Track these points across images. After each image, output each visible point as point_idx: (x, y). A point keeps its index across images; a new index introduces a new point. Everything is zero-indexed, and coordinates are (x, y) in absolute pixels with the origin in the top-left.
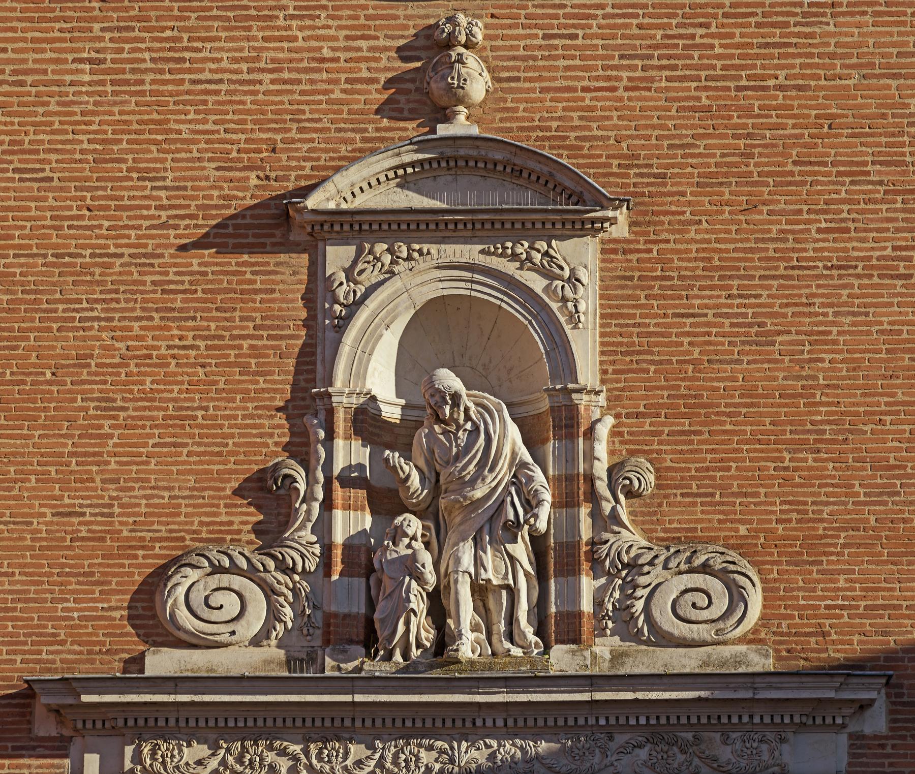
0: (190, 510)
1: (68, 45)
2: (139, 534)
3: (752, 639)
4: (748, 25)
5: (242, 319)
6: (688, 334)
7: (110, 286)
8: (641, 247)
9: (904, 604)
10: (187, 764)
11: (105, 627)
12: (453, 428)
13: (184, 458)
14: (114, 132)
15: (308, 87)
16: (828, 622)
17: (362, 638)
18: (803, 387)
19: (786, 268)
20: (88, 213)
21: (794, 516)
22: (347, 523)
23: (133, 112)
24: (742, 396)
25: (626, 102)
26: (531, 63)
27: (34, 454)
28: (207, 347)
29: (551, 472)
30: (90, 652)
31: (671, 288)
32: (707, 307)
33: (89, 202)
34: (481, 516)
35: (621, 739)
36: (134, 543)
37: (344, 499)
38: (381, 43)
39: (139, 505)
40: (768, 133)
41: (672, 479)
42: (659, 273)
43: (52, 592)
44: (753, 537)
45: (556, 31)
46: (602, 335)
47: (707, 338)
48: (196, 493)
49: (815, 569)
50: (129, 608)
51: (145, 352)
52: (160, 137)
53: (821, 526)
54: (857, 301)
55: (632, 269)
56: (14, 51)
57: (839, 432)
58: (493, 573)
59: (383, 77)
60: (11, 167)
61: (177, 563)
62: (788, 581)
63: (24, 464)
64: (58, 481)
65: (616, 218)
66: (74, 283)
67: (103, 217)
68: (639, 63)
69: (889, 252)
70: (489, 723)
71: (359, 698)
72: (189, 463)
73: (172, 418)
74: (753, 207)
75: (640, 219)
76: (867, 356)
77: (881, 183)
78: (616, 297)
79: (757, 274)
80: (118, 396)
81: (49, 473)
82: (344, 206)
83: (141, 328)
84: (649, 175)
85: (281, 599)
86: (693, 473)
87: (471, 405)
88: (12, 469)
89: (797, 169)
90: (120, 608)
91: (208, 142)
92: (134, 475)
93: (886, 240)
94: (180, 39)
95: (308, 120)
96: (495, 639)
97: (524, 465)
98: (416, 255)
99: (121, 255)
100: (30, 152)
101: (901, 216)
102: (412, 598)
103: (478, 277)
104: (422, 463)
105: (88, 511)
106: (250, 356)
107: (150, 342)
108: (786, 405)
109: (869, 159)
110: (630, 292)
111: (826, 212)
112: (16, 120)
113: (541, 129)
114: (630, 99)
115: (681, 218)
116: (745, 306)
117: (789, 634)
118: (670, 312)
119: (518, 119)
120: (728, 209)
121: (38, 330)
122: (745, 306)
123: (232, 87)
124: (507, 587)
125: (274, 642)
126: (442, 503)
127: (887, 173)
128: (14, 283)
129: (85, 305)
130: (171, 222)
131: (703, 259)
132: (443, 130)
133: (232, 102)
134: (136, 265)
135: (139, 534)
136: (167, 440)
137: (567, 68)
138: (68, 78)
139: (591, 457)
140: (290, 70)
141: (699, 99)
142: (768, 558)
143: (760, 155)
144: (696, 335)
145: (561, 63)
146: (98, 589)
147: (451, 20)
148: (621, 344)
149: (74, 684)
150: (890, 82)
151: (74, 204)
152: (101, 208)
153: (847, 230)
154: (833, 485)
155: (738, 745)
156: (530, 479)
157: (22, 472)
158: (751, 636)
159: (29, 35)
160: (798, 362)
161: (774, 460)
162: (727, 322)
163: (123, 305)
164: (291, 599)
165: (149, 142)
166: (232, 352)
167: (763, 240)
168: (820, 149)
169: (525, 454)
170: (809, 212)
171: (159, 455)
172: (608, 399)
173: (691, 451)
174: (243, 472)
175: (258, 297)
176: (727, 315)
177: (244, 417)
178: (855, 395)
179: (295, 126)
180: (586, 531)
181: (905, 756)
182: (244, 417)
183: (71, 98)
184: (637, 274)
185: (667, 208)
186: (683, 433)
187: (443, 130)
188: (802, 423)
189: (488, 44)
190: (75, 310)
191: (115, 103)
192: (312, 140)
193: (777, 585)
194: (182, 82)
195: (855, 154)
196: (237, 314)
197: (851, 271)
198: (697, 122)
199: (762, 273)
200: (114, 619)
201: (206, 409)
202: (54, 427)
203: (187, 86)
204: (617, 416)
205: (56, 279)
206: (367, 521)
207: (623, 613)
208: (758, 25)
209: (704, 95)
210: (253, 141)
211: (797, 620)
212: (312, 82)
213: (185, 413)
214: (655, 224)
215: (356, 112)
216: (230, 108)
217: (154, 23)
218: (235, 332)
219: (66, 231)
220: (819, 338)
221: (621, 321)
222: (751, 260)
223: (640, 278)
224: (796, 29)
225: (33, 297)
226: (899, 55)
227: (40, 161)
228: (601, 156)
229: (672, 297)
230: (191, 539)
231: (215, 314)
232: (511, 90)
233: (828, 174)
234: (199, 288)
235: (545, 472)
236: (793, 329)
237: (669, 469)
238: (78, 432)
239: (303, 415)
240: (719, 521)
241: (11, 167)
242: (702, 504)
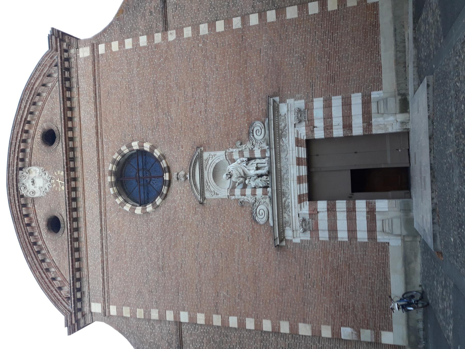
16: (261, 109)
69: (203, 104)
73: (233, 222)
96: (265, 166)
137: (180, 159)
155: (282, 122)
161: (235, 121)
162: (215, 130)
181: (283, 93)
208: (173, 128)
220: (216, 114)
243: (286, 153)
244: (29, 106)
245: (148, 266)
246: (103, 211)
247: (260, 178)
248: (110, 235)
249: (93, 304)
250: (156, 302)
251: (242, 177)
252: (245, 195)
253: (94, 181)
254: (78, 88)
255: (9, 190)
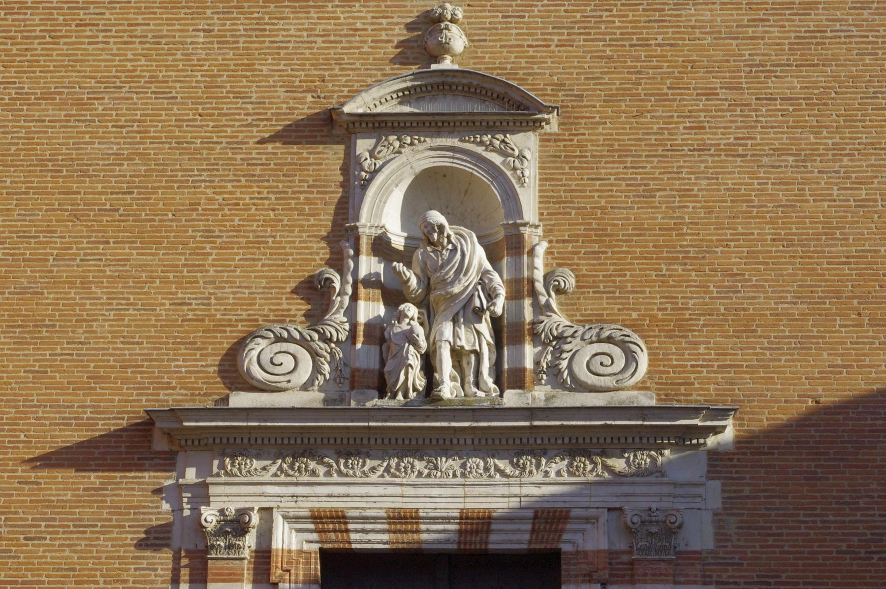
0: (262, 301)
1: (190, 21)
2: (227, 317)
3: (642, 387)
5: (300, 181)
6: (597, 191)
7: (213, 161)
8: (566, 138)
9: (745, 364)
10: (256, 469)
11: (203, 378)
12: (440, 249)
13: (259, 268)
14: (218, 71)
15: (347, 45)
16: (692, 376)
18: (675, 224)
19: (663, 150)
20: (199, 118)
21: (669, 306)
22: (367, 311)
23: (231, 59)
24: (633, 229)
25: (557, 53)
26: (494, 31)
27: (159, 266)
28: (277, 199)
29: (505, 277)
30: (192, 395)
31: (586, 162)
32: (610, 174)
33: (200, 111)
34: (457, 307)
36: (224, 323)
37: (365, 294)
38: (395, 20)
39: (228, 298)
40: (651, 71)
41: (586, 282)
42: (578, 153)
43: (167, 355)
44: (641, 320)
45: (510, 14)
46: (540, 191)
47: (610, 193)
48: (266, 291)
49: (683, 341)
50: (220, 365)
51: (235, 201)
52: (248, 74)
53: (688, 312)
54: (710, 171)
55: (560, 151)
56: (154, 25)
57: (699, 252)
58: (466, 340)
59: (396, 40)
60: (150, 90)
61: (253, 336)
62: (665, 349)
63: (152, 271)
65: (549, 119)
66: (189, 159)
67: (210, 120)
68: (566, 31)
69: (732, 140)
70: (462, 442)
71: (372, 424)
72: (262, 271)
74: (640, 114)
75: (566, 121)
76: (718, 204)
77: (726, 100)
78: (550, 168)
79: (644, 154)
80: (216, 229)
81: (168, 277)
82: (369, 111)
83: (233, 187)
84: (571, 95)
85: (322, 359)
86: (601, 278)
87: (451, 233)
88: (144, 275)
89: (670, 92)
90: (214, 365)
91: (280, 76)
92: (225, 279)
94: (263, 18)
95: (346, 64)
97: (487, 272)
98: (416, 142)
99: (221, 143)
100: (163, 82)
101: (740, 119)
102: (410, 357)
103: (458, 155)
104: (418, 271)
105: (194, 302)
106: (304, 204)
107: (238, 195)
108: (663, 235)
109: (718, 86)
110: (559, 165)
111: (689, 117)
112: (154, 64)
113: (500, 69)
114: (559, 51)
115: (593, 120)
116: (636, 173)
117: (666, 384)
118: (585, 177)
119: (485, 63)
120: (624, 115)
121: (164, 188)
122: (636, 173)
123: (297, 45)
124: (475, 352)
125: (316, 388)
126: (432, 297)
127: (731, 94)
128: (149, 159)
129: (196, 173)
130: (255, 123)
131: (608, 145)
132: (434, 67)
133: (296, 54)
134: (231, 148)
135: (227, 317)
136: (248, 256)
137: (517, 34)
138: (189, 40)
139: (532, 267)
140: (335, 35)
141: (605, 51)
142: (652, 333)
143: (646, 83)
144: (602, 191)
145: (514, 31)
146: (199, 353)
147: (443, 7)
148: (553, 197)
149: (179, 414)
150: (731, 41)
151: (191, 113)
152: (208, 115)
153: (704, 128)
154: (696, 286)
156: (491, 280)
157: (150, 277)
158: (641, 385)
160: (672, 208)
162: (624, 183)
163: (221, 173)
164: (329, 359)
165: (241, 76)
166: (293, 202)
167: (648, 134)
168: (685, 80)
169: (488, 265)
170: (678, 117)
171: (242, 266)
172: (544, 231)
173: (600, 264)
174: (299, 277)
175: (311, 168)
176: (623, 179)
177: (300, 242)
178: (710, 229)
179: (337, 67)
180: (528, 315)
181: (747, 466)
182: (300, 242)
183: (191, 51)
184: (563, 154)
185: (584, 115)
186: (594, 252)
187: (434, 67)
188: (675, 247)
189: (465, 21)
190: (189, 176)
191: (220, 54)
192: (349, 75)
193: (658, 351)
194: (264, 42)
195: (709, 83)
196: (297, 178)
197: (707, 152)
198: (603, 64)
199: (647, 153)
200: (209, 373)
201: (274, 237)
202: (173, 248)
203: (267, 44)
204: (550, 242)
205: (177, 157)
206: (380, 310)
207: (554, 371)
208: (644, 10)
209: (608, 49)
210: (310, 76)
211: (672, 375)
212: (349, 42)
213: (260, 239)
214: (576, 124)
215: (378, 59)
216: (295, 57)
217: (246, 10)
218: (295, 189)
219: (185, 128)
220: (685, 193)
221: (553, 183)
222: (640, 145)
223: (565, 156)
224: (669, 13)
225: (161, 168)
226: (737, 26)
227: (169, 87)
228: (540, 84)
229: (587, 168)
230: (263, 321)
231: (282, 178)
232: (480, 47)
233: (692, 95)
234: (272, 163)
235: (501, 277)
236: (668, 188)
237: (584, 276)
238: (188, 252)
239: (339, 241)
240: (619, 310)
241: (150, 90)
242: (607, 298)
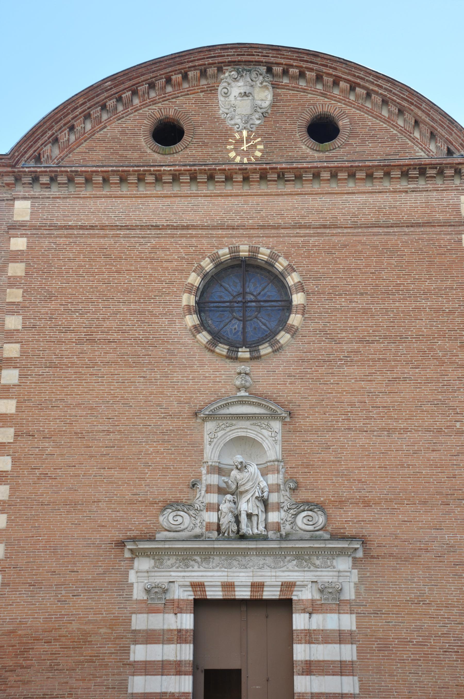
4: (323, 369)
17: (216, 529)
35: (288, 558)
64: (133, 485)
69: (362, 425)
73: (164, 468)
89: (336, 404)
93: (361, 422)
99: (151, 425)
119: (260, 391)
129: (141, 438)
146: (143, 515)
155: (321, 560)
159: (126, 371)
171: (161, 478)
177: (184, 468)
179: (199, 393)
181: (368, 564)
194: (168, 382)
196: (183, 441)
212: (203, 382)
220: (343, 447)
229: (301, 436)
243: (272, 565)
244: (381, 94)
245: (94, 313)
246: (190, 232)
247: (233, 520)
248: (149, 244)
249: (27, 204)
250: (34, 327)
251: (237, 487)
252: (207, 492)
253: (242, 217)
254: (406, 192)
255: (232, 48)
